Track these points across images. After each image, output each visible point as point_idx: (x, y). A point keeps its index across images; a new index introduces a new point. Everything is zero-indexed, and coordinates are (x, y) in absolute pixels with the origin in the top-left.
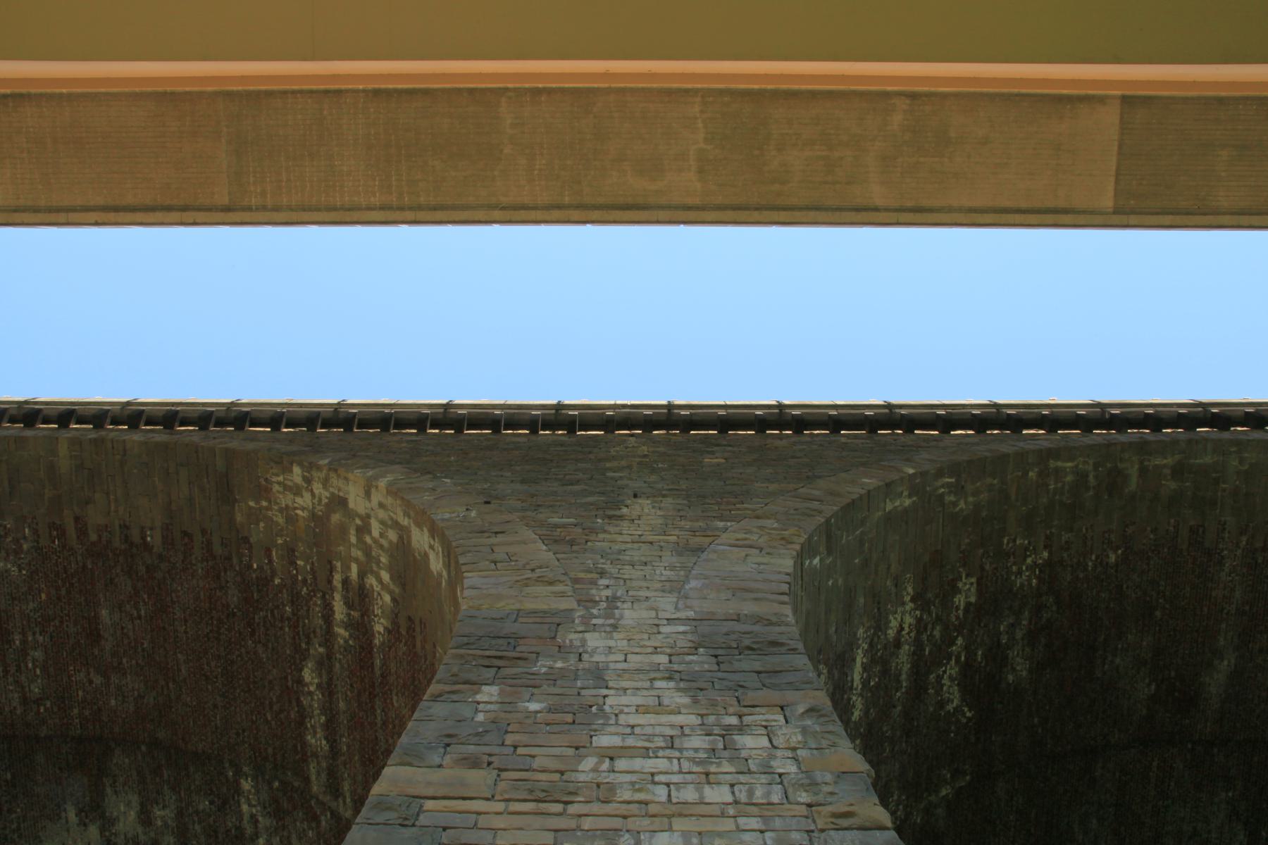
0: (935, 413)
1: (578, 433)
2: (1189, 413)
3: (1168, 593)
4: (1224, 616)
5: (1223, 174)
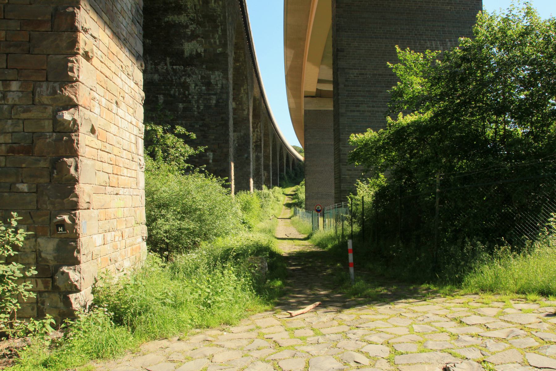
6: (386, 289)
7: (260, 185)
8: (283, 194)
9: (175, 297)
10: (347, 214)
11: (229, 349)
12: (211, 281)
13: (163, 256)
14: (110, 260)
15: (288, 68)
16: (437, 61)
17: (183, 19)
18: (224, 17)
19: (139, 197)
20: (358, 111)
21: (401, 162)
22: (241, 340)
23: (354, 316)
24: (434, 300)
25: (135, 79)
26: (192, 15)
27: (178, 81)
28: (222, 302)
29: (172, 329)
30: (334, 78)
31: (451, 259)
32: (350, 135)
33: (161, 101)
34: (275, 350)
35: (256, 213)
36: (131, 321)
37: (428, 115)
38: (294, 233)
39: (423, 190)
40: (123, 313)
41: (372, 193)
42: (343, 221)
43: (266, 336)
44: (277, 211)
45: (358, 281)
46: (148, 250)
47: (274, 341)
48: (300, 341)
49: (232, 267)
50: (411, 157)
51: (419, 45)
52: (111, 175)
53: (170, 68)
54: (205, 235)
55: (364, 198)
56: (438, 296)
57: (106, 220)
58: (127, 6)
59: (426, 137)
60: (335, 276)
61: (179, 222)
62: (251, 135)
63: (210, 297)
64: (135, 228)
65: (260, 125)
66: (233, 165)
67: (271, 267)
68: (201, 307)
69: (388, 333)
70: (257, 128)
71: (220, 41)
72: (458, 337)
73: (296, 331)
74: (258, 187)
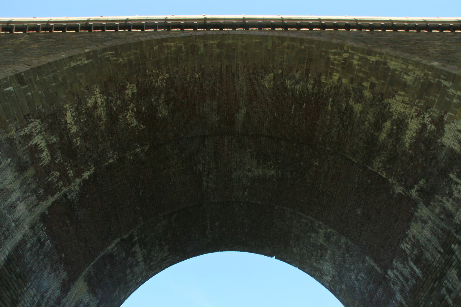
0: (369, 23)
1: (158, 30)
2: (385, 24)
3: (220, 88)
4: (241, 95)
26: (413, 112)
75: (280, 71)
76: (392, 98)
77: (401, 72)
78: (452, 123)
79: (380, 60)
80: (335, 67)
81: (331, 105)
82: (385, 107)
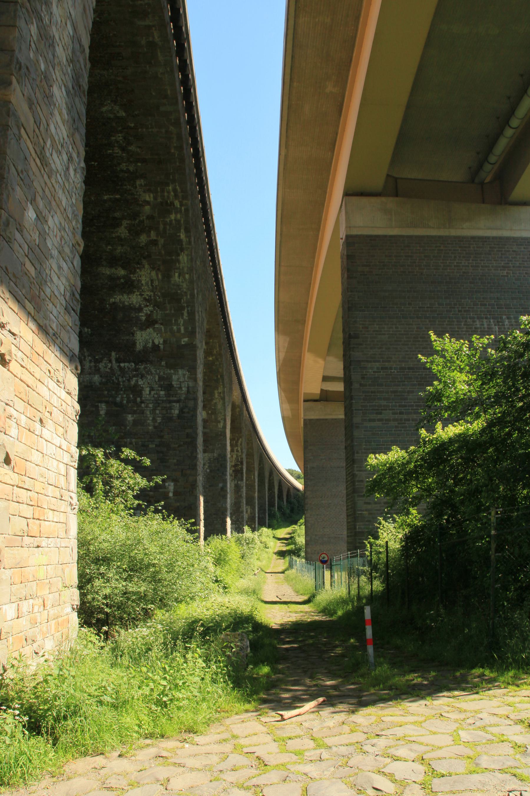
5: (317, 20)
6: (420, 677)
7: (241, 526)
8: (274, 537)
9: (117, 693)
10: (364, 565)
11: (192, 769)
12: (168, 668)
13: (101, 633)
14: (26, 639)
15: (281, 362)
16: (489, 350)
17: (135, 299)
18: (192, 295)
19: (69, 550)
20: (379, 420)
21: (442, 490)
22: (210, 756)
23: (373, 719)
24: (491, 692)
25: (68, 387)
26: (147, 294)
27: (126, 383)
28: (183, 699)
29: (110, 741)
30: (345, 374)
31: (514, 631)
32: (368, 456)
33: (102, 412)
34: (258, 771)
35: (234, 566)
36: (53, 728)
37: (477, 425)
38: (290, 595)
39: (473, 531)
40: (41, 716)
41: (400, 536)
42: (359, 576)
43: (246, 750)
44: (264, 562)
45: (380, 665)
46: (79, 624)
47: (257, 757)
48: (294, 757)
49: (198, 649)
50: (456, 484)
51: (464, 325)
52: (31, 521)
53: (115, 365)
54: (161, 600)
55: (390, 544)
56: (496, 686)
57: (21, 583)
58: (59, 290)
59: (476, 457)
60: (347, 657)
61: (124, 583)
62: (229, 456)
63: (166, 692)
64: (62, 593)
65: (242, 443)
66: (202, 499)
67: (255, 646)
68: (154, 707)
69: (422, 744)
70: (237, 446)
71: (186, 329)
72: (525, 749)
73: (289, 742)
74: (238, 528)
75: (132, 125)
76: (151, 267)
77: (179, 268)
78: (155, 333)
79: (184, 243)
80: (159, 194)
81: (111, 198)
82: (138, 263)
